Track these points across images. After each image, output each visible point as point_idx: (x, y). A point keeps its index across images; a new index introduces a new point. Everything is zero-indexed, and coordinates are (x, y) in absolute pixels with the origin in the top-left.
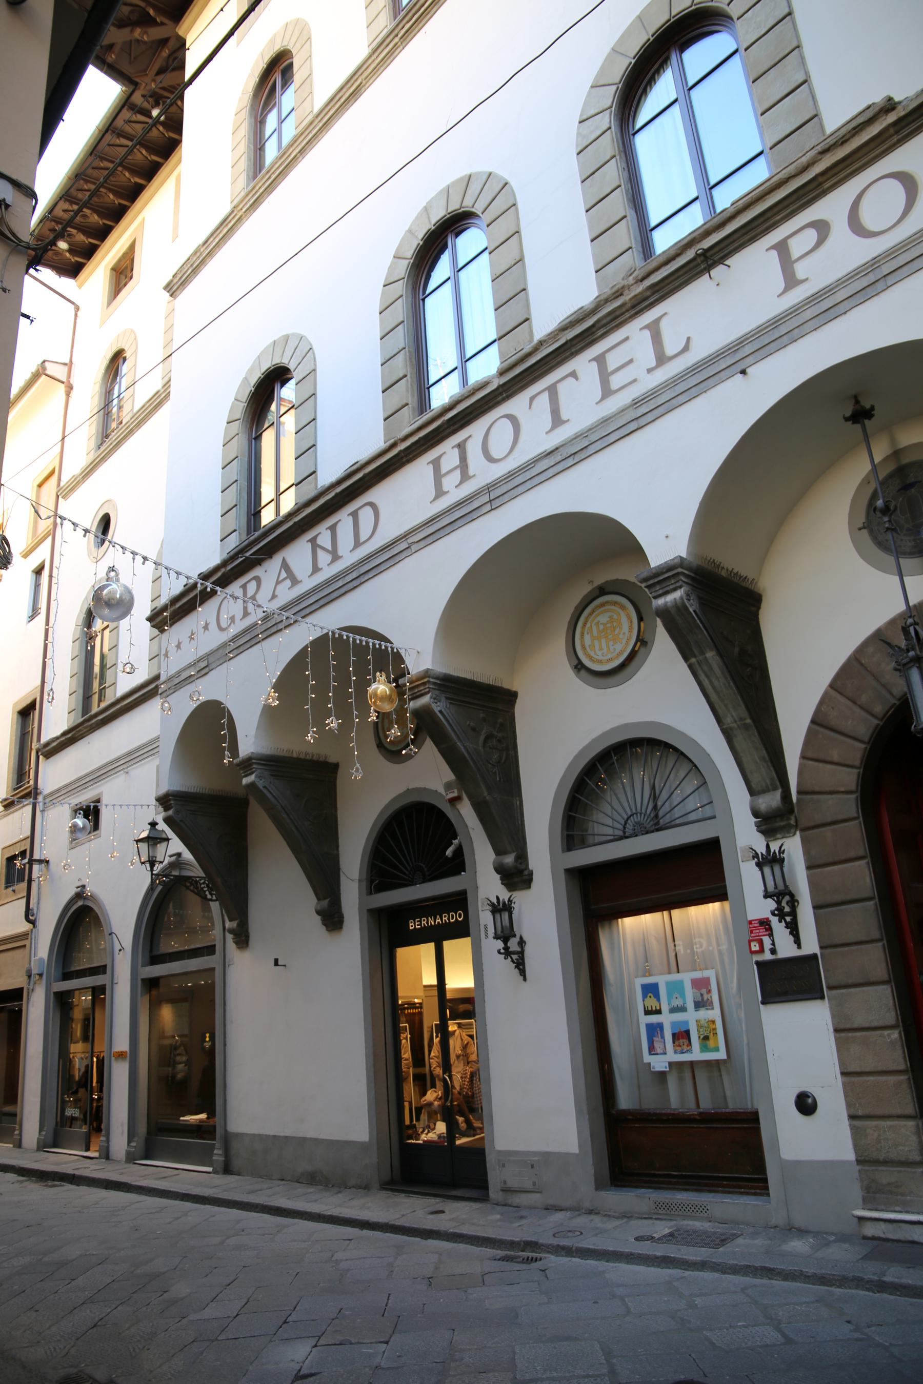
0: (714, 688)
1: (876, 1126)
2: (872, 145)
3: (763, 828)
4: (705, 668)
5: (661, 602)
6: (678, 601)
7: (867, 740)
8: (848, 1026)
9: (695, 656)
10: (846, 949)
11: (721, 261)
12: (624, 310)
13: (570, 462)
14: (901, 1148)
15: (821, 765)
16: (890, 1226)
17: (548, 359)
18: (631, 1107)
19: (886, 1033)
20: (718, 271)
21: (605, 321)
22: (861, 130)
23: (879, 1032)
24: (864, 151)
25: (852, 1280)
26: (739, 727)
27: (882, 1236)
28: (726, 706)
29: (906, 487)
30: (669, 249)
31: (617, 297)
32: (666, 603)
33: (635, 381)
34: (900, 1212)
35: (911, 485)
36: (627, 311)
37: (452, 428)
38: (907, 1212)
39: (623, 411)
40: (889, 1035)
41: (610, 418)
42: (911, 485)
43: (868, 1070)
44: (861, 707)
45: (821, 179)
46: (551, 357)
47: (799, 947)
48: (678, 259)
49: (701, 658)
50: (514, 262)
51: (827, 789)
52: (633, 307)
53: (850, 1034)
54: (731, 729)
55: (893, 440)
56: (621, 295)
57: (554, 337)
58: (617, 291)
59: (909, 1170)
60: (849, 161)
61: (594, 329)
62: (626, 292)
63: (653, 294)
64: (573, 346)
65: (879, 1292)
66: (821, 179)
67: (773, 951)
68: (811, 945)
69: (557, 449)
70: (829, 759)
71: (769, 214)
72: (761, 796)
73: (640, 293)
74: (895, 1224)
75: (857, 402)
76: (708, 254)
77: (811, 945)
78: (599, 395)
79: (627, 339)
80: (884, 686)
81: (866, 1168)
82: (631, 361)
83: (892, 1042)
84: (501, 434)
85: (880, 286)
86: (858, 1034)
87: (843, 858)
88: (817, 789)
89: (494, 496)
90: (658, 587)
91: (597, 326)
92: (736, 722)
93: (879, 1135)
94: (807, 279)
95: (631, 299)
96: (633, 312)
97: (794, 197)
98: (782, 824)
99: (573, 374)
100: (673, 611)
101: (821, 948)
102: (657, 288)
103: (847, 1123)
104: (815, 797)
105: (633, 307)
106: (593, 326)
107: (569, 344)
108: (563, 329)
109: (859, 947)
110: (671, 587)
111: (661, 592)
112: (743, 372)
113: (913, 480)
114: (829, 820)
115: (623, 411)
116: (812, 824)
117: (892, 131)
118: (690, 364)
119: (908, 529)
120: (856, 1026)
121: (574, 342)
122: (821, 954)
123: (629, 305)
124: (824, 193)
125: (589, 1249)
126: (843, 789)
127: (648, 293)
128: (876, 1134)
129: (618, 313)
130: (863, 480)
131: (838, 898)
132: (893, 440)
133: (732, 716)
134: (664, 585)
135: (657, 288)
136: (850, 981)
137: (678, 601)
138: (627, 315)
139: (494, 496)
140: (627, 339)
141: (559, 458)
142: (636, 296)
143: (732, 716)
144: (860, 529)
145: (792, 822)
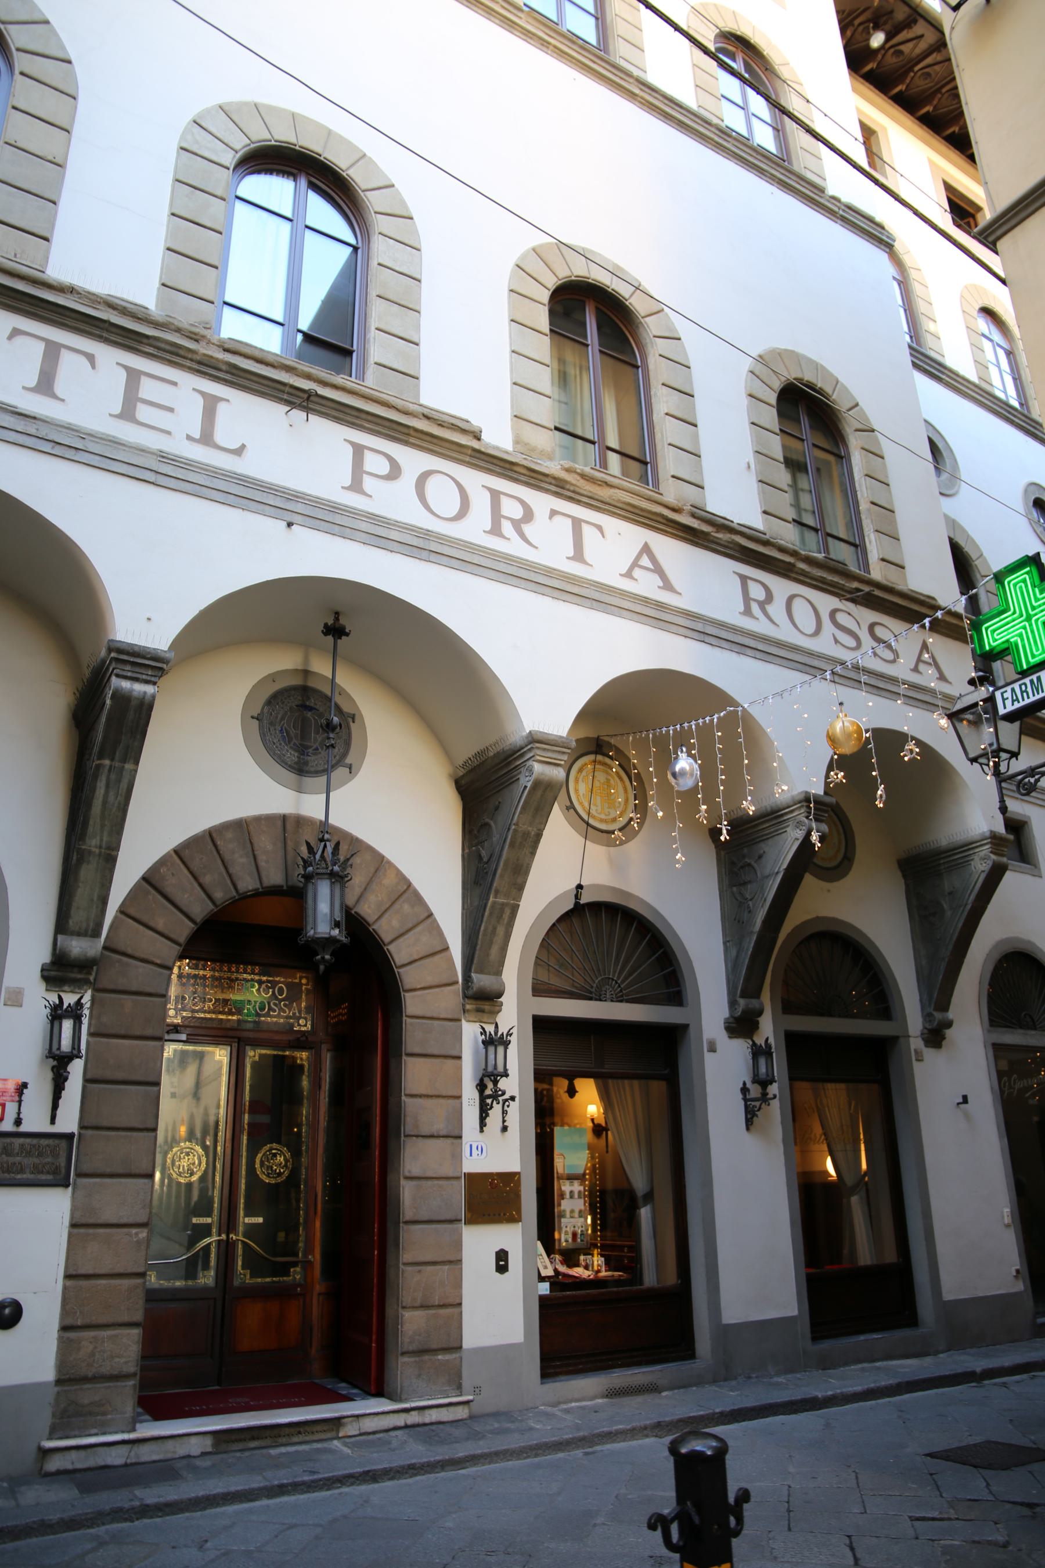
0: (105, 802)
1: (94, 1337)
2: (454, 447)
3: (46, 973)
4: (113, 776)
5: (126, 685)
6: (148, 697)
7: (198, 920)
8: (91, 1221)
9: (112, 760)
10: (113, 1133)
11: (308, 410)
12: (190, 356)
13: (47, 447)
14: (117, 1360)
15: (141, 928)
16: (82, 1453)
17: (68, 313)
18: (875, 1262)
19: (134, 1231)
20: (298, 415)
21: (163, 345)
22: (454, 430)
23: (125, 1230)
24: (447, 445)
25: (109, 1514)
26: (100, 854)
27: (70, 1467)
28: (103, 826)
29: (304, 707)
30: (268, 352)
31: (191, 338)
32: (132, 690)
33: (169, 433)
34: (96, 1435)
35: (311, 709)
36: (191, 360)
37: (228, 377)
38: (104, 1433)
39: (143, 450)
40: (137, 1234)
41: (123, 445)
42: (311, 709)
43: (102, 1272)
44: (201, 885)
45: (412, 432)
46: (73, 315)
47: (53, 1121)
48: (269, 369)
49: (117, 764)
50: (50, 158)
51: (142, 956)
52: (200, 363)
53: (91, 1231)
54: (90, 852)
55: (306, 660)
56: (197, 341)
57: (93, 301)
58: (195, 334)
59: (119, 1384)
60: (435, 441)
61: (145, 341)
62: (203, 343)
63: (227, 372)
64: (107, 331)
65: (138, 1519)
66: (412, 432)
67: (18, 1122)
68: (69, 1121)
69: (35, 418)
70: (152, 924)
71: (363, 416)
72: (75, 937)
73: (217, 359)
74: (89, 1451)
75: (337, 619)
76: (312, 398)
77: (69, 1121)
78: (624, 572)
79: (175, 384)
80: (230, 876)
81: (66, 1388)
82: (171, 410)
83: (138, 1242)
84: (442, 494)
85: (425, 554)
86: (101, 1231)
87: (138, 1033)
88: (130, 951)
89: (380, 533)
90: (128, 668)
91: (151, 341)
92: (101, 847)
93: (96, 1348)
94: (63, 400)
95: (204, 355)
96: (196, 366)
97: (387, 424)
98: (79, 976)
99: (91, 358)
100: (133, 703)
101: (82, 1127)
102: (234, 371)
103: (55, 1335)
104: (125, 959)
105: (200, 363)
106: (147, 337)
107: (107, 325)
108: (110, 305)
109: (129, 1134)
110: (144, 677)
111: (129, 674)
112: (290, 525)
113: (312, 705)
114: (134, 989)
115: (143, 451)
116: (112, 987)
117: (469, 452)
118: (239, 471)
119: (295, 744)
120: (100, 1221)
121: (114, 330)
122: (80, 1134)
123: (198, 358)
124: (406, 443)
125: (694, 1417)
126: (158, 962)
127: (224, 367)
128: (91, 1347)
129: (182, 352)
130: (269, 675)
131: (120, 1075)
132: (306, 660)
133: (101, 840)
134: (137, 669)
135: (234, 371)
136: (108, 1170)
137: (148, 697)
138: (188, 363)
139: (380, 533)
140: (175, 384)
141: (33, 431)
142: (211, 357)
143: (101, 840)
144: (253, 717)
145: (92, 978)
